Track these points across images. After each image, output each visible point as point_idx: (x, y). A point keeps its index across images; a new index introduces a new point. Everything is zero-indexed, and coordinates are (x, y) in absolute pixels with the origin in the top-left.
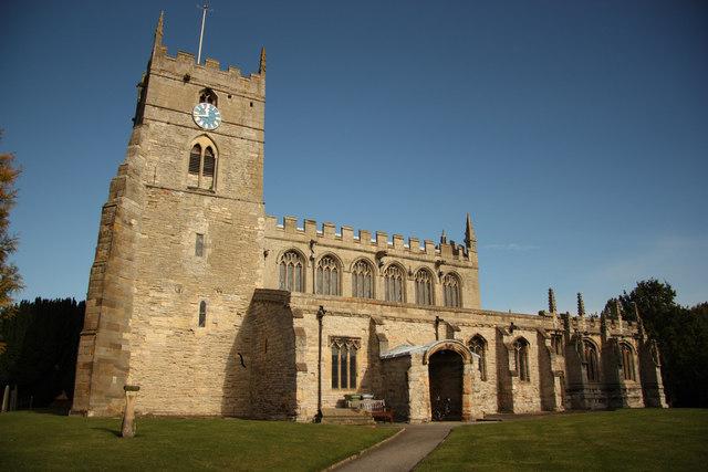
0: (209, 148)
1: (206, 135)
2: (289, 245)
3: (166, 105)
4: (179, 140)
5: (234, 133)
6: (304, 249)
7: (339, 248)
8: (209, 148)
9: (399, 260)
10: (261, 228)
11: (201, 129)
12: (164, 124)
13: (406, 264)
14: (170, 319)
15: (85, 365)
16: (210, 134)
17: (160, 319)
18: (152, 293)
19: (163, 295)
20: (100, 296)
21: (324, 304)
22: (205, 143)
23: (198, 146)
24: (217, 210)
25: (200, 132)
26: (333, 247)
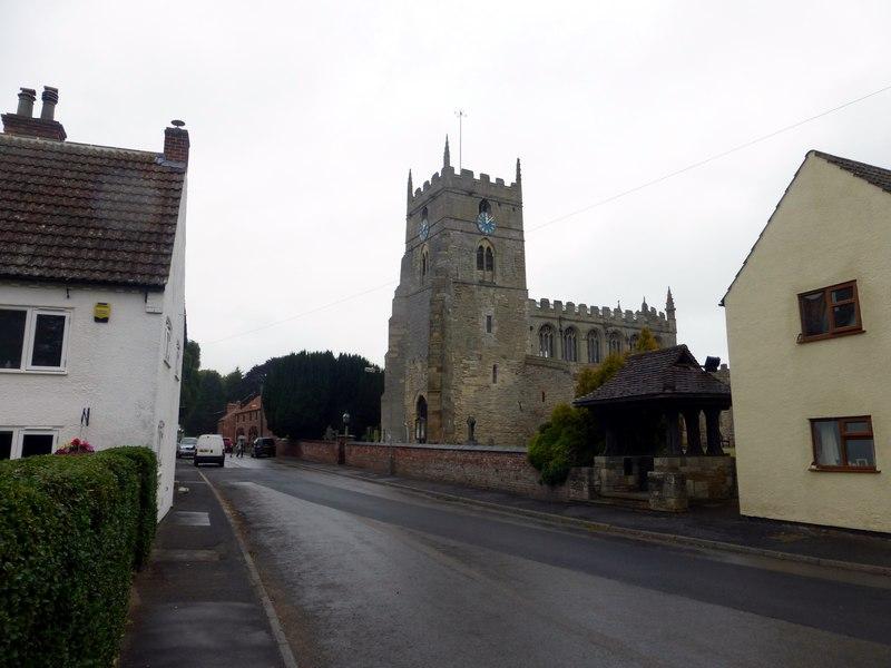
0: (489, 249)
2: (544, 321)
4: (469, 243)
6: (556, 323)
7: (577, 321)
8: (489, 249)
11: (482, 234)
13: (624, 331)
22: (486, 245)
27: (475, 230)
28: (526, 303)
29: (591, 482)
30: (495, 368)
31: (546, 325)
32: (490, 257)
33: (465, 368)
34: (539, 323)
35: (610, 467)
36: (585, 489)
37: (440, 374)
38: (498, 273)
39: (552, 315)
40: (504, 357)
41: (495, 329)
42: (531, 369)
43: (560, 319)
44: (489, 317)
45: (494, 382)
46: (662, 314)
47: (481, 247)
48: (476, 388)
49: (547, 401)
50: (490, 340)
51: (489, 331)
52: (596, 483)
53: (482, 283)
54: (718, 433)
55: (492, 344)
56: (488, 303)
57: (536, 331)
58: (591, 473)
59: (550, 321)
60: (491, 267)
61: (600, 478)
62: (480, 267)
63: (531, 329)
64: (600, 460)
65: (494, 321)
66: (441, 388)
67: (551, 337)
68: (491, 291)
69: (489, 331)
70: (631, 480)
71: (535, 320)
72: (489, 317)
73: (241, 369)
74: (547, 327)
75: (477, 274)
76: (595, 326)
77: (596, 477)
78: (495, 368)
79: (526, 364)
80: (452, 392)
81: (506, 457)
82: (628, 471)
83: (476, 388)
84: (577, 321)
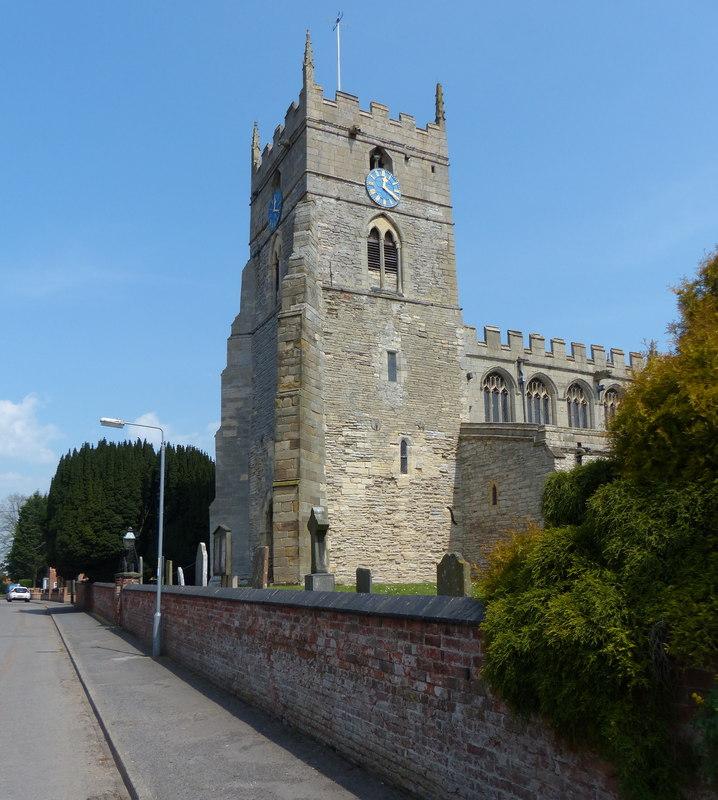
0: (389, 234)
1: (383, 215)
2: (491, 365)
3: (332, 173)
6: (512, 369)
7: (550, 368)
8: (389, 234)
9: (620, 383)
10: (460, 342)
11: (376, 206)
12: (333, 201)
14: (368, 464)
15: (286, 525)
16: (389, 214)
17: (358, 464)
18: (346, 432)
19: (358, 434)
20: (294, 435)
21: (582, 439)
22: (383, 226)
23: (375, 232)
24: (409, 319)
25: (378, 212)
26: (543, 366)
27: (363, 197)
30: (404, 443)
32: (392, 250)
33: (348, 445)
37: (295, 453)
38: (407, 278)
40: (422, 428)
41: (403, 375)
44: (392, 354)
45: (404, 470)
47: (375, 232)
48: (370, 482)
49: (501, 503)
50: (395, 394)
51: (393, 377)
53: (376, 294)
55: (399, 402)
56: (390, 325)
57: (478, 379)
60: (393, 266)
62: (374, 263)
63: (469, 377)
65: (401, 361)
66: (299, 476)
68: (395, 306)
69: (393, 377)
72: (392, 354)
74: (496, 375)
75: (370, 279)
76: (580, 376)
78: (404, 443)
80: (323, 487)
81: (388, 635)
83: (370, 482)
84: (550, 368)
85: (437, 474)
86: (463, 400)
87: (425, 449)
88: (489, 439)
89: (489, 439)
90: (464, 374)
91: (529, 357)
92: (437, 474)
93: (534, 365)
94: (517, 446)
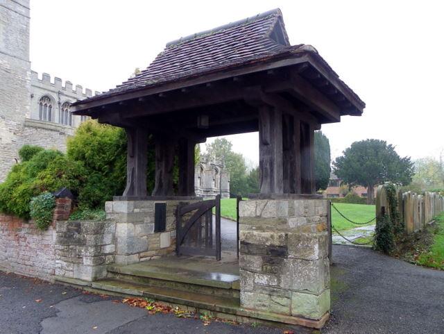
2: (45, 93)
5: (10, 7)
6: (55, 96)
28: (29, 73)
29: (99, 247)
31: (67, 102)
34: (39, 94)
35: (133, 218)
36: (87, 261)
39: (52, 89)
42: (28, 131)
43: (59, 93)
46: (132, 157)
52: (108, 249)
54: (83, 101)
58: (99, 231)
59: (50, 93)
61: (115, 240)
64: (118, 207)
67: (50, 107)
70: (165, 240)
71: (37, 89)
73: (411, 160)
77: (108, 239)
79: (25, 126)
82: (160, 227)
85: (10, 142)
86: (28, 107)
87: (4, 129)
88: (39, 128)
89: (39, 128)
90: (29, 94)
91: (65, 92)
92: (10, 142)
93: (66, 96)
94: (53, 133)
